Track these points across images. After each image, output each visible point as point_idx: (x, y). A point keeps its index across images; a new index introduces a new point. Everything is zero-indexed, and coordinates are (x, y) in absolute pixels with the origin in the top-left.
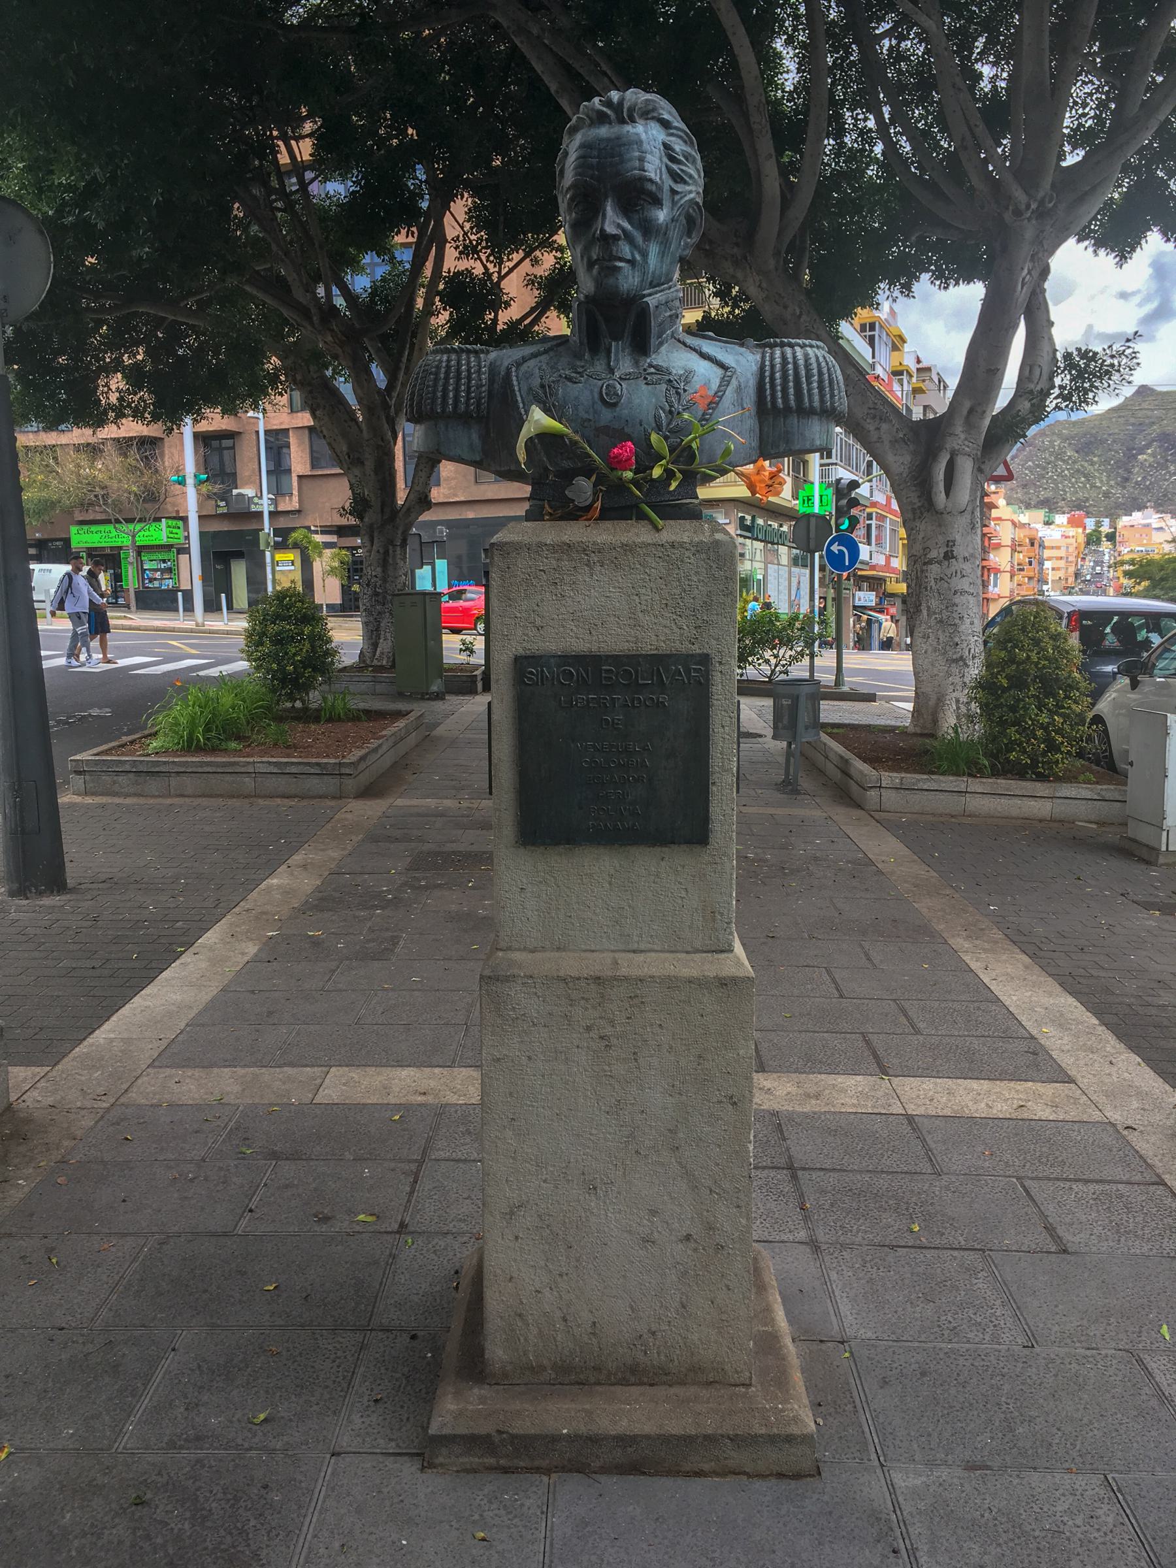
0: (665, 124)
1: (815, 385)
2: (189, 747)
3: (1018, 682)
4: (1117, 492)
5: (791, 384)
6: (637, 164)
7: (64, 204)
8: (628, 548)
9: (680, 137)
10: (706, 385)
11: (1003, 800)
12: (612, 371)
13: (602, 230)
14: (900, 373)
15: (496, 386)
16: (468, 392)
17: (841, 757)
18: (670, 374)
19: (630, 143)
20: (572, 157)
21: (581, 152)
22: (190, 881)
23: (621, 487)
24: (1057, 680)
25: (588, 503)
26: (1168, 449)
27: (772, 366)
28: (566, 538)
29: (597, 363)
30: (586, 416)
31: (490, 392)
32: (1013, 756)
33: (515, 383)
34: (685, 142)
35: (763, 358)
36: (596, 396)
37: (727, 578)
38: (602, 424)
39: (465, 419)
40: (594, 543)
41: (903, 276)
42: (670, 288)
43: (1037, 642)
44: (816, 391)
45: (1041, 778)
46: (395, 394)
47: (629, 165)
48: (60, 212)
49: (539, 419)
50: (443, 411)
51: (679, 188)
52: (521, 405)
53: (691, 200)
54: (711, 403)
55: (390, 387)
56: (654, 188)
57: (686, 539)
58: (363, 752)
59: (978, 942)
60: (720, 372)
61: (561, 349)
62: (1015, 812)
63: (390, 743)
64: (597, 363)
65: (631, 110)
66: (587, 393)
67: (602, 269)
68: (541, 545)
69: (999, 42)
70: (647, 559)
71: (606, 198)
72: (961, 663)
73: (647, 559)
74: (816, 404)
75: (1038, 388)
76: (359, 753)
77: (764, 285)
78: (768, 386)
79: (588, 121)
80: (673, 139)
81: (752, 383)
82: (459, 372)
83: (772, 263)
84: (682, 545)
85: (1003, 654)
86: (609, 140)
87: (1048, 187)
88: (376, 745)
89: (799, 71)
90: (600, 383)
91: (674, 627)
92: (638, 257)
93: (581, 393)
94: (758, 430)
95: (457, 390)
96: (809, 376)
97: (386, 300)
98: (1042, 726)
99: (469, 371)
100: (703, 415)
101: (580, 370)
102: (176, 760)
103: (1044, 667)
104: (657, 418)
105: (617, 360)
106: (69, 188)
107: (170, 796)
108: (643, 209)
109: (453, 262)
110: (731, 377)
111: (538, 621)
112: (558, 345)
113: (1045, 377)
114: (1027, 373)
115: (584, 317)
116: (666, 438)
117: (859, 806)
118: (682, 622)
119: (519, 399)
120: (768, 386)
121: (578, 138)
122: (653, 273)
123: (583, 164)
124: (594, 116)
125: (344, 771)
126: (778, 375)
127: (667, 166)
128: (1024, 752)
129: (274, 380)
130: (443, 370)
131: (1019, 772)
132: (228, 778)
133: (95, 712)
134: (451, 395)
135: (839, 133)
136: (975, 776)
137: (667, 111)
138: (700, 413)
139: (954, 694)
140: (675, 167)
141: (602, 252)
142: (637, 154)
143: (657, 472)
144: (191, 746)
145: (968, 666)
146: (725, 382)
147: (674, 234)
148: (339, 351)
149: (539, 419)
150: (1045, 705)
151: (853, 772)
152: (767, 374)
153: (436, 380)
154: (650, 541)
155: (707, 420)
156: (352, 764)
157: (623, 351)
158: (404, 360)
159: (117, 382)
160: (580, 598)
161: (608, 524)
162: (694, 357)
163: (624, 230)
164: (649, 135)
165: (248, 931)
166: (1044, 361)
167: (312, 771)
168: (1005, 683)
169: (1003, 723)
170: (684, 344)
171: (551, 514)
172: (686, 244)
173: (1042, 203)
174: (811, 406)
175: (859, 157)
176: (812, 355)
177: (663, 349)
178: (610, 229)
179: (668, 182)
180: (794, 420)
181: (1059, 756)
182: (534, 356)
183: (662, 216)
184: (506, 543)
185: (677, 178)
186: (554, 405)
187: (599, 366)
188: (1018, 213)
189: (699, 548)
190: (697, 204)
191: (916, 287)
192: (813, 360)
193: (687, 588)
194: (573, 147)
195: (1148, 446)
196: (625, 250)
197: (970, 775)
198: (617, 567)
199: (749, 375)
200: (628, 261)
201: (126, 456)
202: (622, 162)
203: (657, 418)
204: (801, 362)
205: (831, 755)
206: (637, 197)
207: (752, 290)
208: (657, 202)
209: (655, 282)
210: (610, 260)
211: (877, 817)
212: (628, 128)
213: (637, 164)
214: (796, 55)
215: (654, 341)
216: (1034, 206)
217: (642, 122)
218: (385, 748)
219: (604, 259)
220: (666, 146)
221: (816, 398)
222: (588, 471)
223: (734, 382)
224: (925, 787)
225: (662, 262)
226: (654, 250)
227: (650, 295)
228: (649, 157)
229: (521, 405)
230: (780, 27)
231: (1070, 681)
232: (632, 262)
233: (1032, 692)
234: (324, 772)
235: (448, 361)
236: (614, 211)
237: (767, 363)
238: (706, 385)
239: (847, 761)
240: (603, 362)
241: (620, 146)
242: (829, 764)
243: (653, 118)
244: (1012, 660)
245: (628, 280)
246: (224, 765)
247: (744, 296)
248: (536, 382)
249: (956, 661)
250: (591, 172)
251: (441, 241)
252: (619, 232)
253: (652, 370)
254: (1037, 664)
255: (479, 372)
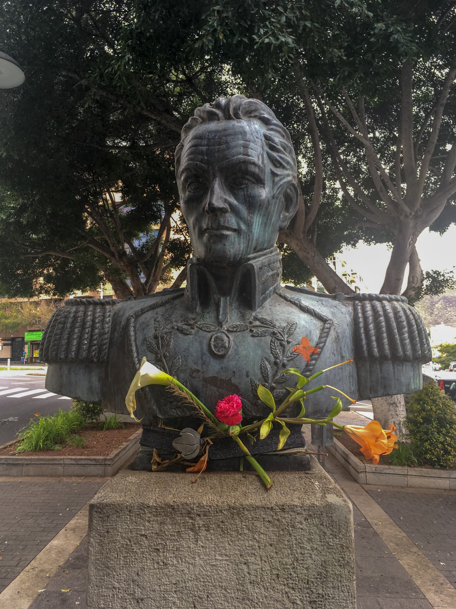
0: (266, 122)
1: (406, 335)
2: (36, 449)
3: (427, 420)
4: (429, 317)
5: (385, 335)
6: (242, 150)
7: (11, 214)
8: (236, 511)
9: (279, 132)
10: (307, 338)
11: (426, 479)
12: (220, 324)
13: (210, 204)
14: (346, 275)
15: (116, 334)
16: (91, 339)
17: (344, 452)
18: (274, 326)
19: (235, 134)
20: (187, 146)
21: (193, 142)
22: (11, 542)
23: (227, 441)
24: (445, 419)
25: (195, 455)
26: (446, 302)
27: (365, 318)
28: (170, 499)
29: (207, 316)
30: (195, 367)
31: (111, 339)
32: (428, 456)
33: (132, 333)
34: (283, 136)
35: (355, 309)
36: (205, 347)
37: (342, 546)
38: (210, 375)
39: (87, 363)
40: (200, 506)
41: (352, 241)
42: (271, 252)
43: (434, 401)
44: (408, 341)
45: (443, 467)
46: (148, 285)
47: (234, 151)
48: (8, 217)
49: (149, 370)
50: (66, 357)
51: (278, 171)
52: (135, 355)
53: (289, 182)
54: (313, 354)
55: (147, 282)
56: (257, 170)
57: (297, 502)
58: (118, 450)
59: (442, 596)
60: (319, 324)
61: (177, 302)
62: (432, 485)
63: (133, 443)
64: (207, 316)
65: (236, 110)
66: (197, 344)
67: (211, 237)
68: (143, 507)
69: (385, 156)
70: (257, 524)
71: (214, 177)
72: (394, 405)
73: (256, 523)
74: (409, 352)
75: (417, 286)
76: (115, 452)
77: (299, 244)
78: (363, 336)
79: (200, 120)
80: (272, 133)
81: (348, 332)
82: (84, 322)
83: (302, 236)
84: (292, 508)
85: (419, 407)
86: (216, 132)
87: (419, 206)
88: (125, 446)
89: (308, 167)
90: (209, 335)
91: (286, 601)
92: (243, 227)
93: (190, 345)
94: (355, 375)
95: (80, 338)
96: (400, 328)
97: (147, 249)
98: (441, 443)
99: (93, 320)
100: (307, 365)
101: (192, 322)
102: (27, 458)
103: (439, 414)
104: (263, 370)
105: (225, 314)
106: (13, 208)
107: (22, 476)
108: (247, 187)
109: (173, 236)
110: (329, 328)
111: (138, 593)
112: (174, 298)
113: (419, 281)
114: (411, 280)
115: (196, 276)
116: (272, 389)
117: (355, 480)
118: (296, 596)
119: (134, 349)
120: (363, 336)
121: (192, 134)
122: (257, 240)
123: (195, 151)
124: (205, 116)
125: (107, 462)
126: (371, 326)
127: (268, 153)
128: (433, 454)
129: (101, 278)
130: (70, 320)
131: (431, 464)
132: (51, 467)
133: (11, 419)
134: (75, 342)
135: (324, 188)
136: (411, 467)
137: (267, 113)
138: (304, 364)
139: (393, 420)
140: (275, 154)
141: (211, 223)
142: (241, 142)
143: (265, 430)
144: (36, 449)
145: (398, 407)
146: (324, 333)
147: (275, 208)
148: (126, 269)
149: (149, 370)
150: (441, 432)
151: (350, 462)
152: (361, 325)
153: (63, 329)
154: (259, 504)
155: (310, 371)
156: (112, 459)
157: (231, 305)
158: (153, 271)
159: (41, 280)
160: (183, 566)
161: (214, 479)
162: (295, 310)
163: (230, 205)
164: (253, 128)
165: (29, 588)
166: (418, 275)
167: (92, 463)
168: (421, 420)
169: (423, 441)
170: (285, 298)
171: (159, 464)
172: (285, 217)
173: (416, 212)
174: (405, 355)
175: (333, 198)
176: (400, 309)
177: (267, 303)
178: (217, 203)
179: (269, 167)
180: (389, 367)
181: (450, 457)
182: (153, 307)
183: (264, 193)
184: (107, 505)
185: (276, 163)
186: (165, 356)
187: (209, 319)
188: (406, 216)
189: (312, 513)
190: (293, 185)
191: (357, 245)
192: (402, 313)
193: (300, 557)
194: (187, 141)
195: (439, 301)
196: (232, 221)
197: (409, 466)
198: (224, 532)
199: (345, 326)
200: (234, 230)
201: (49, 306)
202: (228, 148)
203: (263, 370)
204: (391, 315)
205: (338, 450)
206: (240, 177)
207: (294, 246)
208: (260, 182)
209: (258, 248)
210: (217, 229)
211: (366, 489)
212: (235, 123)
213: (242, 150)
214: (307, 162)
215: (258, 297)
216: (413, 214)
217: (245, 118)
218: (130, 446)
219: (213, 228)
220: (267, 138)
221: (409, 347)
222: (195, 422)
223: (333, 334)
224: (387, 472)
225: (265, 231)
226: (257, 221)
227: (254, 258)
228: (252, 145)
229: (135, 355)
230: (300, 152)
231: (452, 420)
232: (238, 231)
233: (435, 425)
234: (97, 463)
235: (76, 312)
236: (219, 185)
237: (360, 315)
238: (307, 338)
239: (347, 455)
240: (213, 315)
241: (226, 136)
242: (337, 454)
243: (255, 117)
244: (424, 410)
245: (234, 246)
246: (49, 460)
247: (289, 248)
248: (151, 333)
249: (392, 404)
250: (200, 157)
251: (169, 228)
252: (226, 206)
253: (257, 323)
254: (435, 412)
255: (103, 321)
